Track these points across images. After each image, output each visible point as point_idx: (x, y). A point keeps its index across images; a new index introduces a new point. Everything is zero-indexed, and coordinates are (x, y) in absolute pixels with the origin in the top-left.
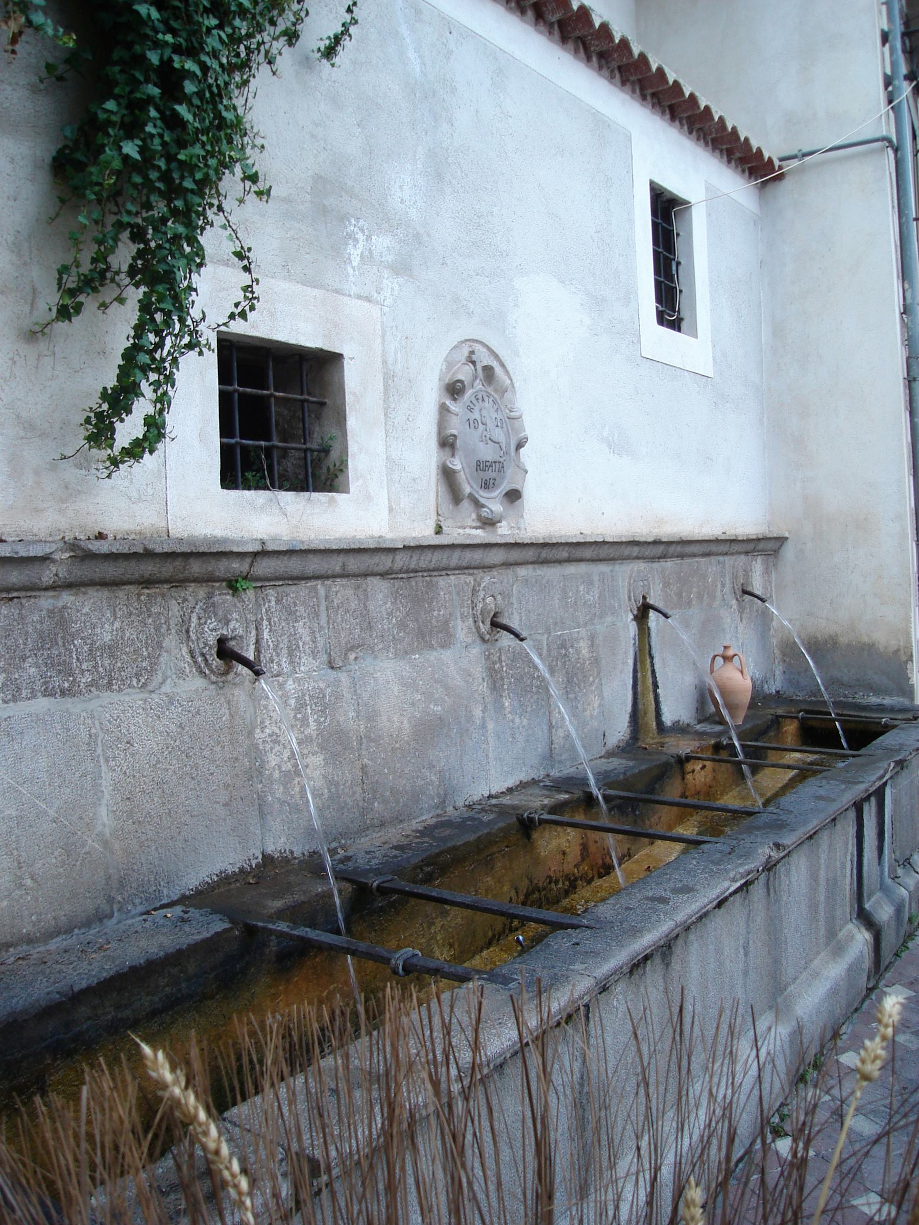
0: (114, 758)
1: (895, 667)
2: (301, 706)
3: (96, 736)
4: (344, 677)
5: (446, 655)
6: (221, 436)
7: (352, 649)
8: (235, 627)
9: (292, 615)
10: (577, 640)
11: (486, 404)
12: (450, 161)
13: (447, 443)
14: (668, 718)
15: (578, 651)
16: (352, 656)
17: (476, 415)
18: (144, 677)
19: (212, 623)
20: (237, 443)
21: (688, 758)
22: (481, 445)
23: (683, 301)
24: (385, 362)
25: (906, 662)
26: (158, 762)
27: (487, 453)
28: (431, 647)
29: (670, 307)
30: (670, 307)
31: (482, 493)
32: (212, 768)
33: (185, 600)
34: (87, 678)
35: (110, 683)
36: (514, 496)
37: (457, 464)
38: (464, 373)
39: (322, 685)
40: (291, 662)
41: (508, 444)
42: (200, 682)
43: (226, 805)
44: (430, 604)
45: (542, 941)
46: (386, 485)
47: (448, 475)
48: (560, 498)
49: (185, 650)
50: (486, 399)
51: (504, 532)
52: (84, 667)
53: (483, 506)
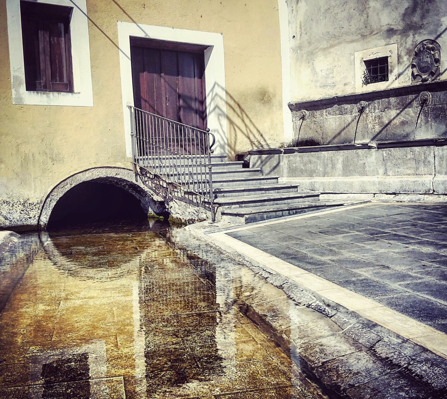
4: (384, 113)
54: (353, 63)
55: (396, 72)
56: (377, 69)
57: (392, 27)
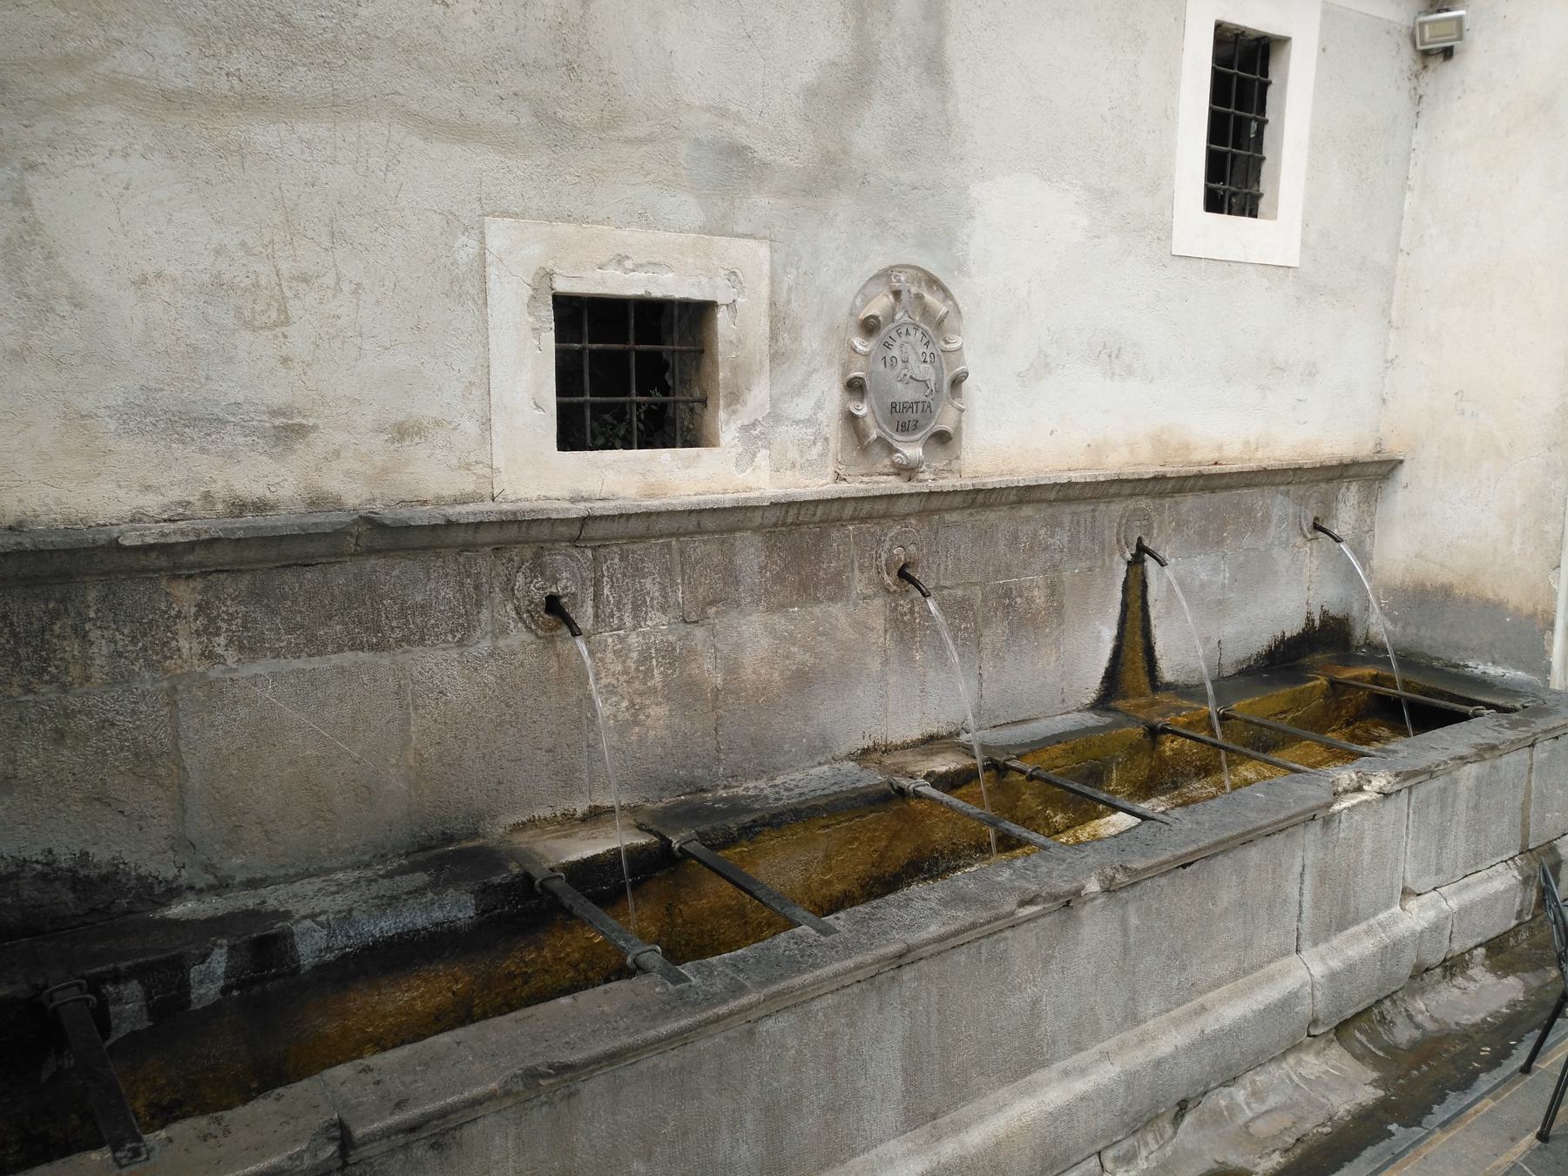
0: (424, 707)
1: (1529, 633)
2: (645, 658)
3: (407, 685)
4: (699, 633)
5: (836, 609)
6: (558, 395)
7: (712, 603)
8: (564, 585)
9: (639, 572)
10: (1030, 589)
11: (911, 338)
12: (882, 57)
13: (855, 387)
14: (1168, 670)
15: (1030, 601)
16: (712, 611)
17: (895, 352)
18: (464, 632)
19: (539, 582)
20: (583, 349)
21: (1164, 731)
22: (899, 385)
23: (1254, 165)
24: (773, 304)
25: (1543, 631)
26: (474, 709)
27: (908, 394)
28: (817, 601)
29: (1234, 178)
30: (1234, 178)
31: (897, 437)
32: (535, 717)
33: (510, 560)
34: (398, 634)
35: (422, 639)
36: (942, 438)
37: (862, 410)
38: (879, 306)
39: (671, 638)
40: (635, 617)
41: (939, 381)
42: (529, 637)
43: (549, 751)
44: (819, 555)
45: (703, 956)
46: (762, 447)
47: (851, 419)
48: (1015, 430)
49: (509, 607)
50: (912, 331)
51: (928, 481)
52: (394, 624)
53: (897, 451)
54: (473, 285)
55: (759, 396)
56: (630, 366)
57: (741, 134)
